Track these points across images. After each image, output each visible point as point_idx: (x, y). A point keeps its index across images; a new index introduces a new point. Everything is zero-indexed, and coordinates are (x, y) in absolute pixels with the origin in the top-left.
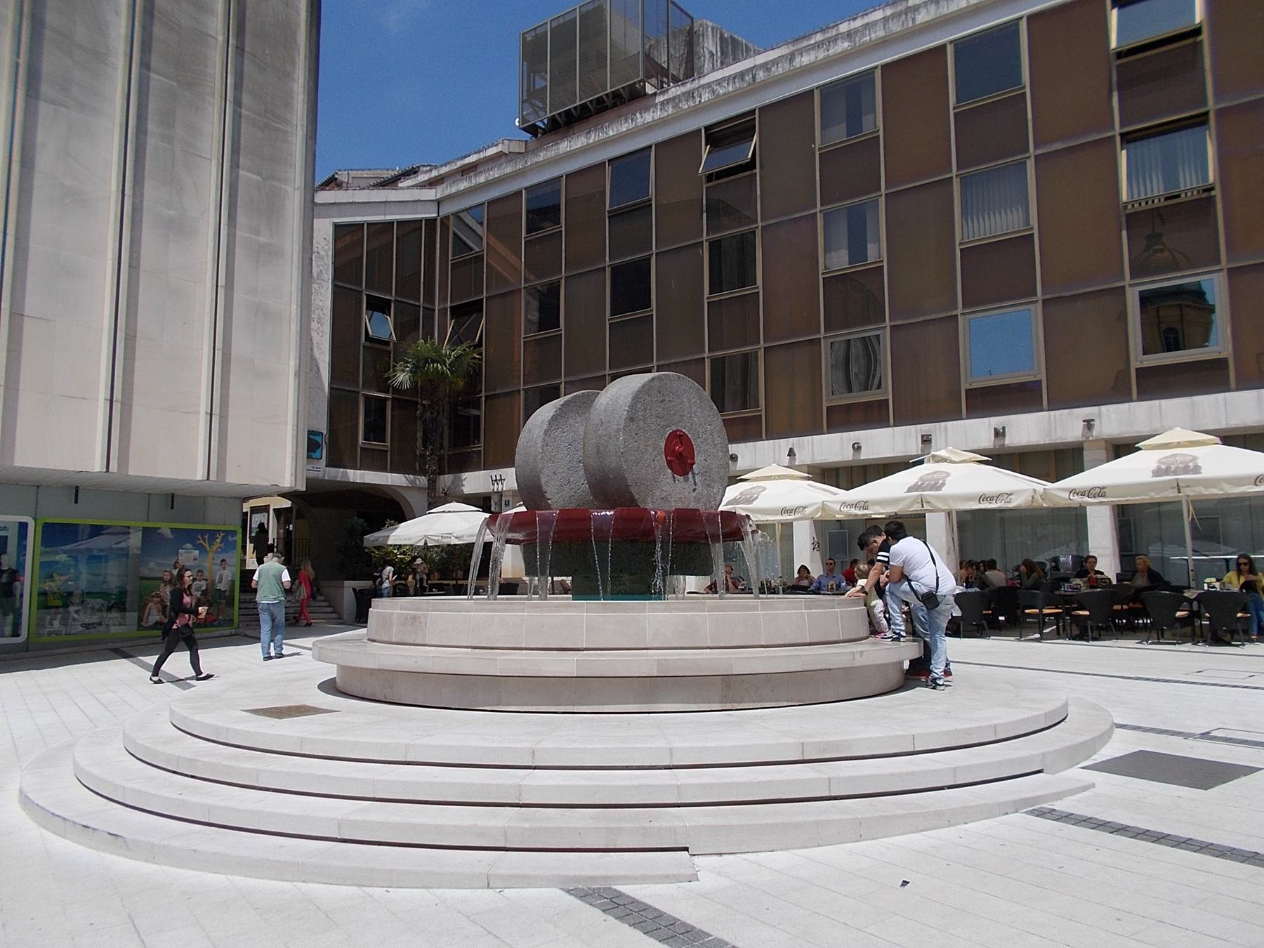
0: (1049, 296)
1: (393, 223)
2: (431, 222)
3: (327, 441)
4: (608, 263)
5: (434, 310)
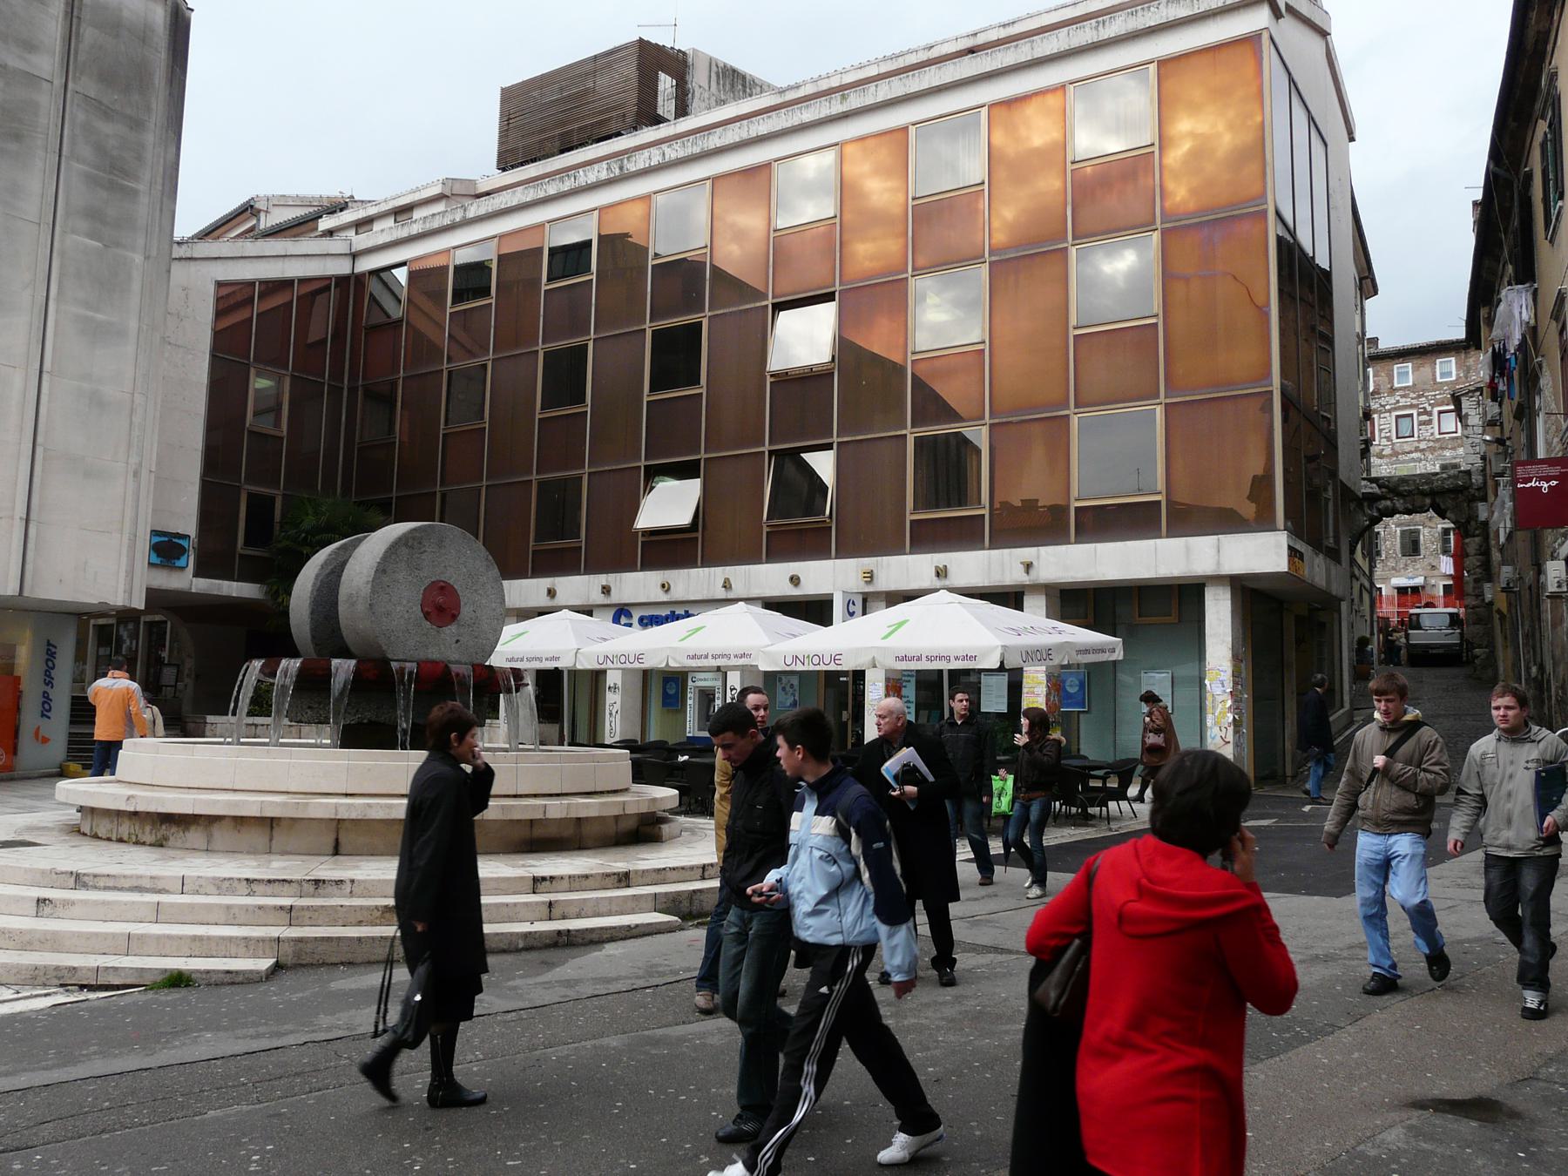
0: (997, 421)
1: (293, 281)
2: (342, 281)
3: (196, 546)
4: (491, 356)
5: (343, 388)
